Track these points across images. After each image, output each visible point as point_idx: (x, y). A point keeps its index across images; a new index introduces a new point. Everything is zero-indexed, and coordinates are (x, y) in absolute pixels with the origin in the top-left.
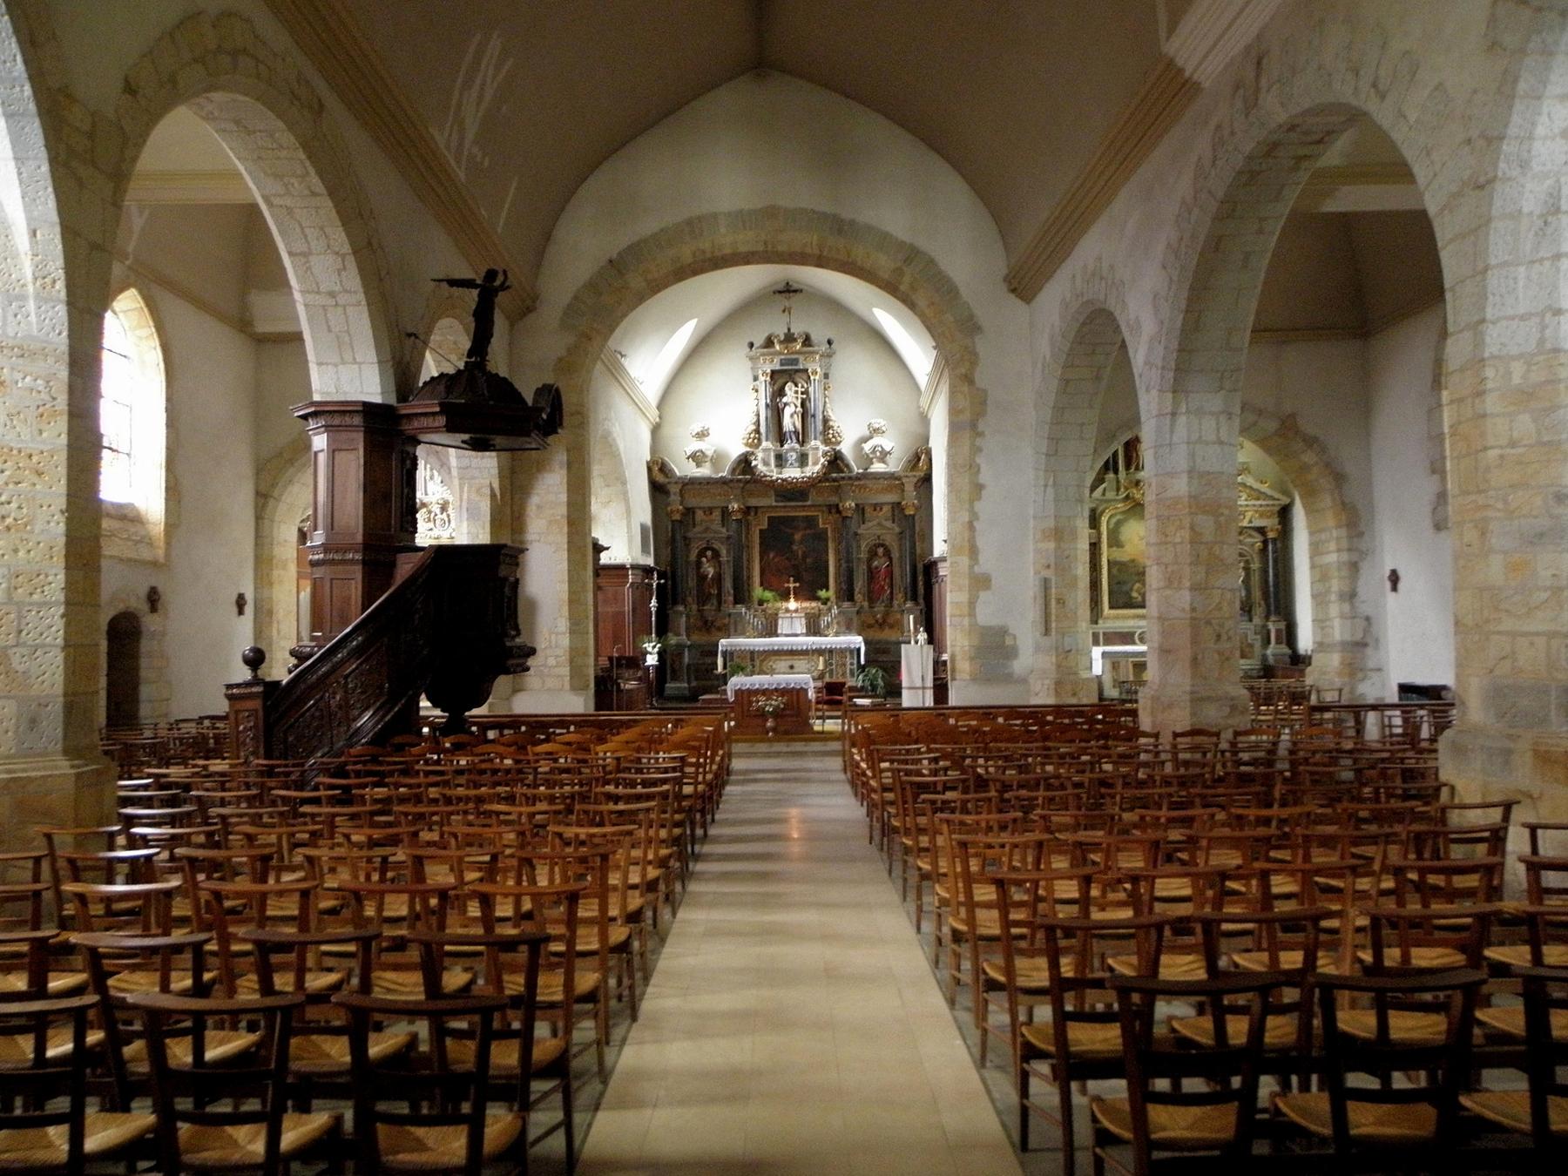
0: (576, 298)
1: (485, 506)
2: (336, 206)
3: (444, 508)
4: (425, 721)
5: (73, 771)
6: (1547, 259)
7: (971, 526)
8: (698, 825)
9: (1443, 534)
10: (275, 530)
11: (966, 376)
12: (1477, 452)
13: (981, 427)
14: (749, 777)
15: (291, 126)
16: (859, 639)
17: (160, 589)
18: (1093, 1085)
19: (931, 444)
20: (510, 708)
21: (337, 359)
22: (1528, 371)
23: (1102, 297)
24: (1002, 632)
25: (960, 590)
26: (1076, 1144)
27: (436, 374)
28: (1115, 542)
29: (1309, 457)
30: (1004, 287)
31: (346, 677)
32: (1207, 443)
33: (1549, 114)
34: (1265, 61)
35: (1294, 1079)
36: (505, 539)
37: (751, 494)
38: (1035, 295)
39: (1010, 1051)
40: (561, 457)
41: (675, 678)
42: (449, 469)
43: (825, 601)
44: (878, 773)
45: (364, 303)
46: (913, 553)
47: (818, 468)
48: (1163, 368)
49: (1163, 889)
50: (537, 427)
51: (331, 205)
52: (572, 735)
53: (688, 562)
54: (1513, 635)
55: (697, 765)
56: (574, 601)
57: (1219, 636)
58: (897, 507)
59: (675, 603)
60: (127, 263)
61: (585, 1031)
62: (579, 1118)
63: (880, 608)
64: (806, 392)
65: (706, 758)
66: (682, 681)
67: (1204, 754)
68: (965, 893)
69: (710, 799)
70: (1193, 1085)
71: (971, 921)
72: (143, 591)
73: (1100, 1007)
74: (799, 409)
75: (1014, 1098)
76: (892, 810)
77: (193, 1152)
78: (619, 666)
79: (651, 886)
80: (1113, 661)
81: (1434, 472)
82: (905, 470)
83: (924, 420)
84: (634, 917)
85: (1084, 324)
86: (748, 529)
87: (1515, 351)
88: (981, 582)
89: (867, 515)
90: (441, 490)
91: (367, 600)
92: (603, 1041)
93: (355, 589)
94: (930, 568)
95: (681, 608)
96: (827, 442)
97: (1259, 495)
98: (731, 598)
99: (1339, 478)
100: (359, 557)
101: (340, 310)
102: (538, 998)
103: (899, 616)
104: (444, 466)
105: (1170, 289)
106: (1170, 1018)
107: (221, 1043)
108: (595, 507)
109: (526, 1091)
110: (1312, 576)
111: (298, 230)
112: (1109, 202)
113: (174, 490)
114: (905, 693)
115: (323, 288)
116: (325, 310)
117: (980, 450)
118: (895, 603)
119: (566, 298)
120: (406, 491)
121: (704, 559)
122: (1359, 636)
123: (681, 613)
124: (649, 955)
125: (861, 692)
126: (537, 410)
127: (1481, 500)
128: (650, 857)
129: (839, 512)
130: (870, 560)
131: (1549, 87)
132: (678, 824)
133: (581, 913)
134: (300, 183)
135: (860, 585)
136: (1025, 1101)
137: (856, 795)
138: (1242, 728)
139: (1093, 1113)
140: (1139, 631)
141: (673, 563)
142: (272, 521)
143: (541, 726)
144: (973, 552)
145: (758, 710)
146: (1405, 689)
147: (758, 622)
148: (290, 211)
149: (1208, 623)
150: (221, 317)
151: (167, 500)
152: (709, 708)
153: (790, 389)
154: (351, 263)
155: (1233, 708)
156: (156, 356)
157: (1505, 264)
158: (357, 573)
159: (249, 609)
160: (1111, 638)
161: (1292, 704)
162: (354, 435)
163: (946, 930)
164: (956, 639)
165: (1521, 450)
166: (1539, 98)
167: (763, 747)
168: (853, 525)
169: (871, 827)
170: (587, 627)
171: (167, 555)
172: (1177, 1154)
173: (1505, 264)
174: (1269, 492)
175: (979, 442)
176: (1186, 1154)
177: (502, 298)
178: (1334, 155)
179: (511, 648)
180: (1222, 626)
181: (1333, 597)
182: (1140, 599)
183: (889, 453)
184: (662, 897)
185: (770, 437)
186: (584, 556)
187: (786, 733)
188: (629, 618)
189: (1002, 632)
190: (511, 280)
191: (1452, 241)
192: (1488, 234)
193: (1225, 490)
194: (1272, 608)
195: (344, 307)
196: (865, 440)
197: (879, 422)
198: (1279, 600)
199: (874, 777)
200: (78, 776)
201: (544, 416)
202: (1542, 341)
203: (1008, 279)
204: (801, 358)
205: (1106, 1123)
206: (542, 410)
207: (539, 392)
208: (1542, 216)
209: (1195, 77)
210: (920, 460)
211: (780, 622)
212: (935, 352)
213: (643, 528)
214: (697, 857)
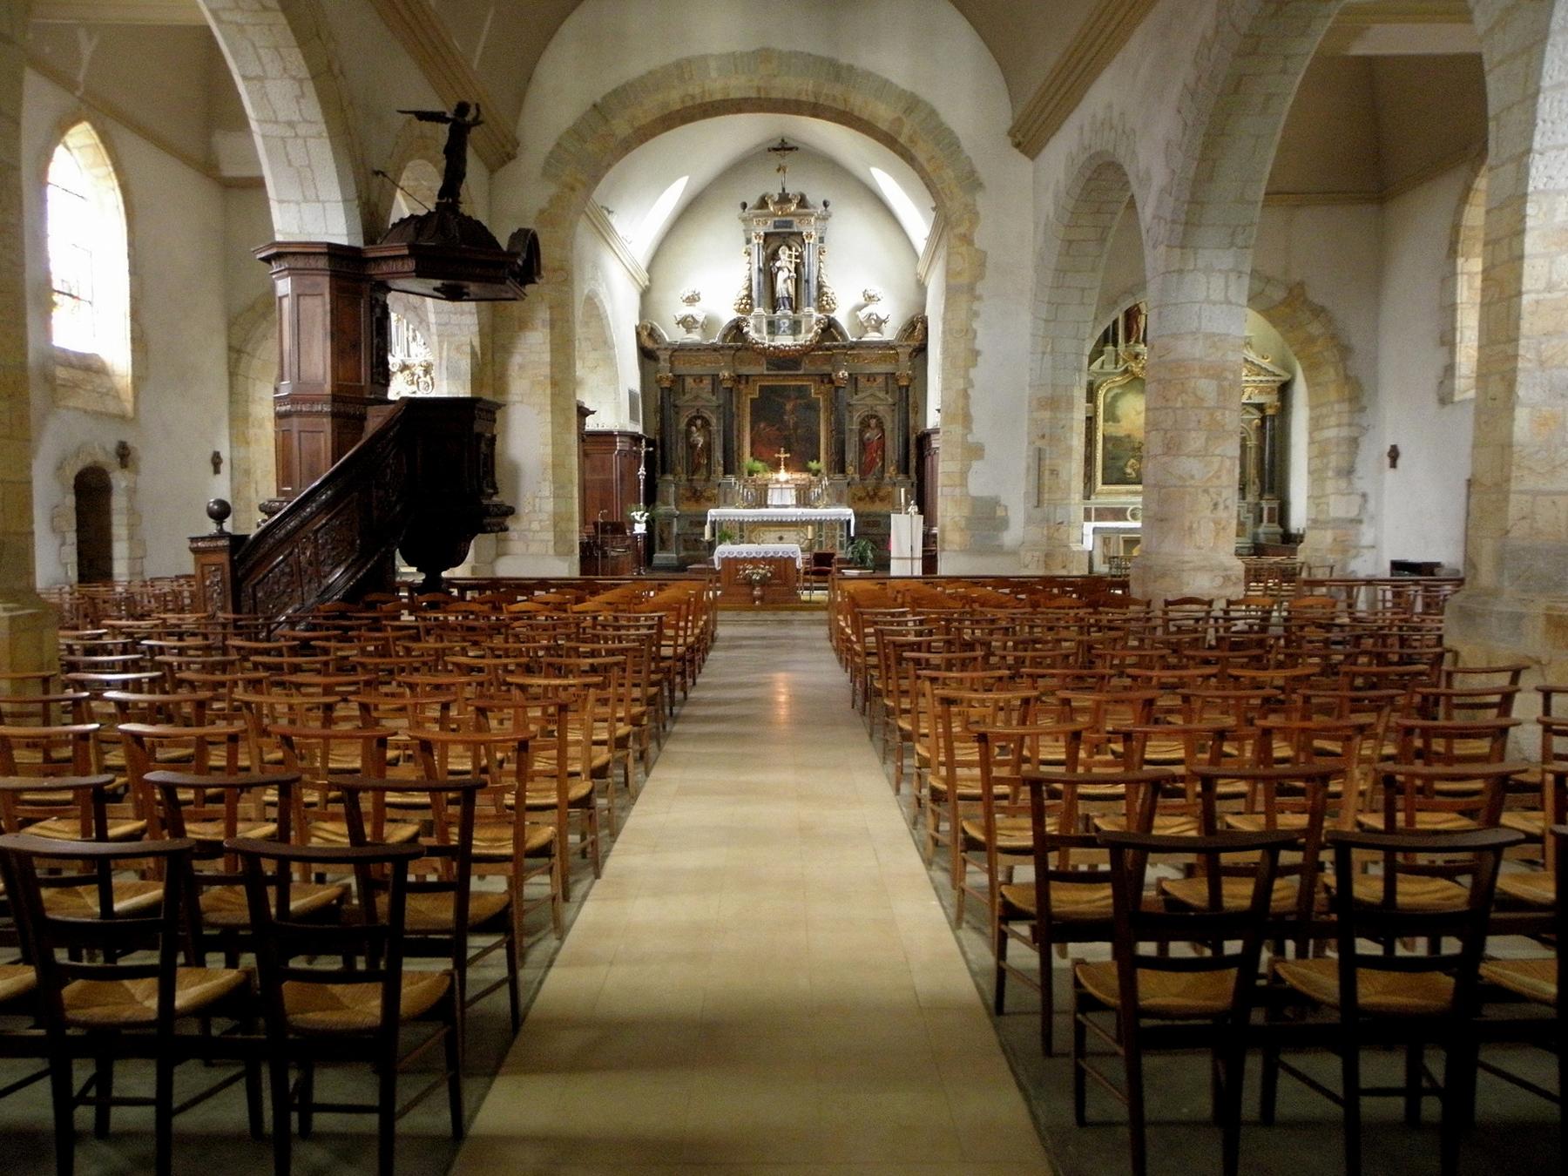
0: (558, 145)
2: (290, 23)
3: (427, 371)
5: (6, 614)
7: (965, 395)
8: (678, 688)
9: (1449, 408)
10: (251, 390)
11: (965, 236)
12: (1511, 297)
13: (980, 288)
14: (734, 644)
16: (850, 511)
17: (131, 442)
18: (1075, 949)
19: (927, 313)
20: (493, 572)
21: (300, 198)
24: (994, 503)
25: (952, 459)
26: (1056, 1007)
27: (407, 214)
28: (1111, 416)
29: (1315, 329)
30: (1009, 140)
35: (1290, 946)
36: (487, 395)
37: (742, 362)
38: (1040, 150)
39: (988, 911)
40: (543, 314)
41: (664, 547)
43: (816, 473)
44: (862, 637)
45: (325, 134)
47: (811, 335)
48: (1173, 222)
50: (514, 275)
51: (285, 22)
52: (552, 596)
53: (678, 432)
54: (1535, 494)
57: (1216, 505)
59: (664, 472)
60: (78, 94)
61: (538, 886)
62: (525, 974)
63: (871, 481)
65: (687, 621)
66: (669, 551)
68: (946, 752)
69: (692, 659)
70: (1180, 949)
71: (951, 780)
72: (112, 446)
73: (1083, 868)
74: (793, 274)
75: (990, 960)
76: (875, 673)
77: (80, 1008)
79: (621, 743)
80: (1105, 537)
81: (1443, 343)
82: (900, 338)
83: (921, 287)
84: (599, 773)
85: (1089, 180)
86: (739, 397)
88: (975, 451)
89: (860, 385)
90: (424, 352)
91: (336, 455)
93: (325, 441)
94: (924, 439)
95: (670, 477)
96: (821, 309)
97: (1261, 370)
98: (721, 469)
99: (1345, 351)
100: (327, 409)
101: (300, 141)
105: (1184, 134)
106: (1160, 880)
108: (580, 371)
110: (1310, 451)
111: (250, 49)
112: (1124, 41)
113: (140, 341)
114: (893, 563)
115: (282, 116)
117: (976, 314)
119: (550, 145)
121: (694, 428)
123: (671, 482)
126: (511, 254)
129: (831, 382)
130: (861, 432)
135: (851, 456)
136: (1001, 963)
138: (1233, 598)
140: (1131, 507)
141: (662, 430)
144: (967, 420)
146: (1398, 566)
148: (241, 28)
149: (1206, 491)
150: (186, 159)
151: (134, 351)
153: (784, 253)
154: (309, 88)
155: (1227, 578)
156: (115, 199)
158: (326, 424)
159: (225, 468)
160: (1102, 514)
161: (1282, 582)
162: (319, 279)
163: (925, 792)
164: (948, 509)
168: (845, 395)
169: (854, 691)
170: (571, 491)
171: (136, 409)
172: (1168, 1022)
174: (1271, 368)
175: (976, 305)
177: (475, 134)
179: (488, 505)
180: (1219, 494)
181: (1330, 474)
182: (1134, 475)
183: (885, 321)
188: (616, 488)
189: (994, 503)
190: (484, 115)
191: (1501, 63)
195: (305, 138)
196: (860, 308)
197: (874, 289)
199: (858, 641)
200: (12, 619)
201: (520, 262)
204: (796, 220)
205: (1091, 989)
206: (518, 255)
207: (514, 237)
210: (916, 328)
211: (770, 492)
212: (934, 214)
213: (632, 394)
214: (674, 718)
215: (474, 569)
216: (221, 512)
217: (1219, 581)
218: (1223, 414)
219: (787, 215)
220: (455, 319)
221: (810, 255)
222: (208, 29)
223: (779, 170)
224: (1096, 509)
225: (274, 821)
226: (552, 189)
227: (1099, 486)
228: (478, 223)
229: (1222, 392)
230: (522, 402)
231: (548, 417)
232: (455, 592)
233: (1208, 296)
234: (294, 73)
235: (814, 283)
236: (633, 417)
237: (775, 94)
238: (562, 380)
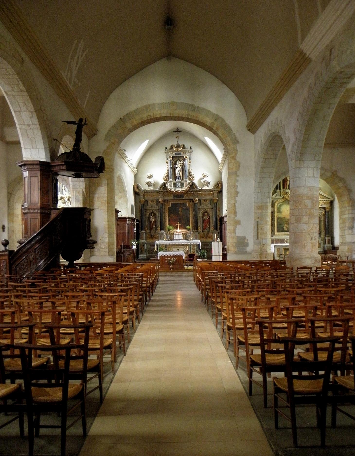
3: (69, 199)
7: (234, 205)
13: (238, 173)
14: (164, 283)
15: (13, 67)
18: (273, 374)
20: (89, 261)
21: (31, 147)
23: (277, 131)
24: (244, 238)
25: (231, 225)
27: (63, 152)
28: (279, 211)
29: (340, 184)
30: (246, 129)
31: (36, 249)
34: (333, 50)
37: (166, 196)
38: (256, 132)
40: (105, 182)
42: (69, 185)
43: (189, 229)
45: (39, 128)
46: (216, 215)
48: (297, 153)
49: (295, 314)
50: (97, 170)
55: (147, 278)
57: (312, 238)
59: (142, 230)
61: (107, 358)
62: (104, 385)
63: (206, 232)
64: (183, 164)
74: (181, 169)
75: (247, 379)
76: (209, 291)
78: (124, 248)
79: (131, 313)
82: (214, 189)
83: (220, 173)
84: (125, 322)
88: (238, 223)
91: (42, 225)
92: (115, 360)
93: (38, 221)
94: (222, 219)
95: (144, 231)
96: (190, 179)
98: (159, 228)
100: (39, 211)
101: (31, 130)
102: (89, 347)
103: (212, 234)
104: (67, 184)
108: (116, 199)
109: (86, 377)
110: (340, 222)
112: (281, 99)
114: (213, 257)
115: (26, 123)
116: (27, 131)
117: (237, 181)
120: (54, 190)
124: (130, 335)
125: (199, 257)
126: (96, 164)
128: (131, 304)
129: (193, 201)
130: (203, 217)
132: (140, 295)
133: (106, 320)
134: (17, 87)
135: (199, 224)
136: (251, 379)
137: (198, 287)
138: (318, 267)
139: (274, 382)
140: (286, 239)
141: (141, 217)
143: (100, 265)
144: (235, 213)
145: (167, 262)
147: (168, 236)
149: (309, 234)
152: (152, 262)
153: (178, 163)
155: (316, 261)
158: (39, 216)
159: (6, 230)
160: (277, 241)
163: (226, 327)
164: (230, 240)
167: (168, 274)
169: (202, 296)
170: (114, 236)
175: (237, 178)
176: (306, 396)
177: (84, 128)
180: (313, 235)
181: (346, 228)
183: (209, 183)
184: (135, 317)
187: (176, 269)
188: (127, 234)
189: (244, 238)
193: (315, 192)
194: (327, 232)
197: (206, 173)
201: (98, 166)
203: (247, 126)
204: (182, 153)
206: (98, 164)
209: (310, 57)
210: (219, 185)
212: (224, 151)
213: (132, 206)
215: (83, 260)
216: (6, 243)
217: (313, 261)
218: (313, 211)
221: (186, 163)
222: (4, 97)
223: (176, 138)
226: (108, 144)
227: (276, 233)
229: (313, 203)
232: (78, 267)
236: (132, 213)
237: (175, 115)
238: (111, 202)
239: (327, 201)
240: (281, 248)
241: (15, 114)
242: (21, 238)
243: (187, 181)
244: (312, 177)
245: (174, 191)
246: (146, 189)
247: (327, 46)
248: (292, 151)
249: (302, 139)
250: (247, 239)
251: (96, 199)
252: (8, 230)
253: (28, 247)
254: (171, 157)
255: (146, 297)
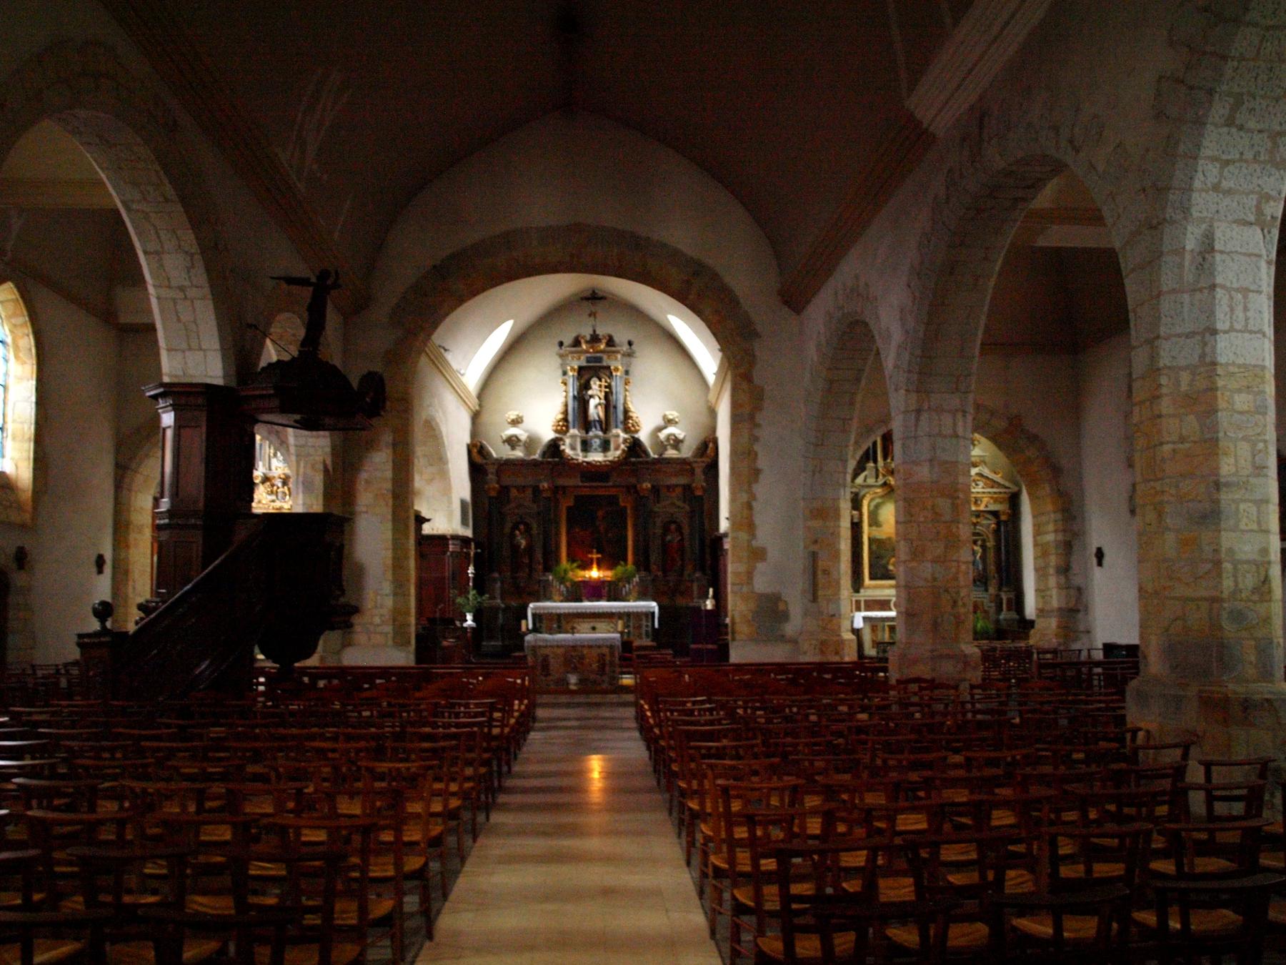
1: (319, 480)
3: (285, 483)
4: (262, 672)
6: (1205, 288)
7: (749, 506)
10: (133, 498)
12: (1155, 446)
13: (759, 418)
14: (551, 726)
16: (653, 606)
20: (340, 660)
21: (184, 346)
22: (1193, 380)
27: (274, 359)
28: (874, 522)
29: (1031, 453)
32: (945, 437)
33: (1203, 171)
36: (337, 511)
40: (387, 438)
41: (491, 638)
47: (618, 453)
48: (909, 372)
54: (1185, 600)
56: (398, 564)
58: (687, 488)
63: (672, 577)
64: (609, 386)
67: (947, 705)
72: (12, 550)
74: (603, 401)
79: (451, 815)
83: (713, 413)
87: (1183, 363)
95: (496, 575)
96: (626, 430)
97: (994, 483)
101: (188, 303)
104: (282, 445)
107: (48, 950)
108: (418, 482)
110: (1035, 553)
113: (41, 461)
116: (175, 304)
118: (686, 573)
121: (517, 532)
122: (1071, 605)
127: (1158, 485)
129: (636, 492)
131: (1202, 150)
142: (130, 490)
148: (147, 216)
149: (947, 591)
153: (595, 384)
157: (1174, 291)
159: (108, 568)
160: (871, 605)
165: (1187, 445)
166: (1195, 158)
173: (1174, 291)
174: (1002, 482)
178: (1045, 198)
180: (958, 593)
181: (1051, 571)
183: (682, 441)
185: (576, 425)
186: (407, 527)
191: (1133, 270)
192: (1160, 266)
196: (660, 429)
197: (672, 414)
198: (1009, 574)
202: (1203, 356)
203: (780, 293)
204: (605, 357)
208: (1200, 253)
209: (932, 128)
210: (708, 447)
212: (720, 354)
213: (463, 503)
214: (502, 789)
215: (322, 659)
216: (104, 611)
217: (960, 666)
218: (958, 528)
219: (598, 352)
220: (311, 441)
221: (617, 385)
222: (117, 212)
223: (590, 315)
224: (865, 601)
225: (1094, 675)
227: (867, 581)
228: (334, 366)
229: (955, 507)
230: (367, 512)
231: (389, 525)
232: (306, 679)
233: (940, 431)
234: (186, 249)
235: (620, 408)
236: (464, 522)
238: (402, 492)
239: (1001, 496)
240: (882, 624)
241: (147, 259)
242: (148, 596)
243: (619, 434)
244: (951, 437)
245: (584, 462)
246: (505, 457)
247: (972, 108)
248: (896, 366)
249: (921, 334)
250: (786, 602)
251: (360, 486)
252: (114, 568)
253: (166, 622)
254: (576, 367)
255: (499, 766)
